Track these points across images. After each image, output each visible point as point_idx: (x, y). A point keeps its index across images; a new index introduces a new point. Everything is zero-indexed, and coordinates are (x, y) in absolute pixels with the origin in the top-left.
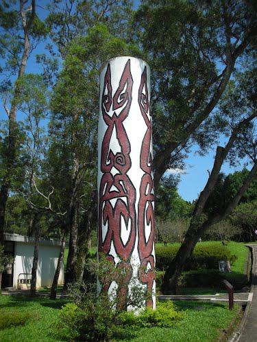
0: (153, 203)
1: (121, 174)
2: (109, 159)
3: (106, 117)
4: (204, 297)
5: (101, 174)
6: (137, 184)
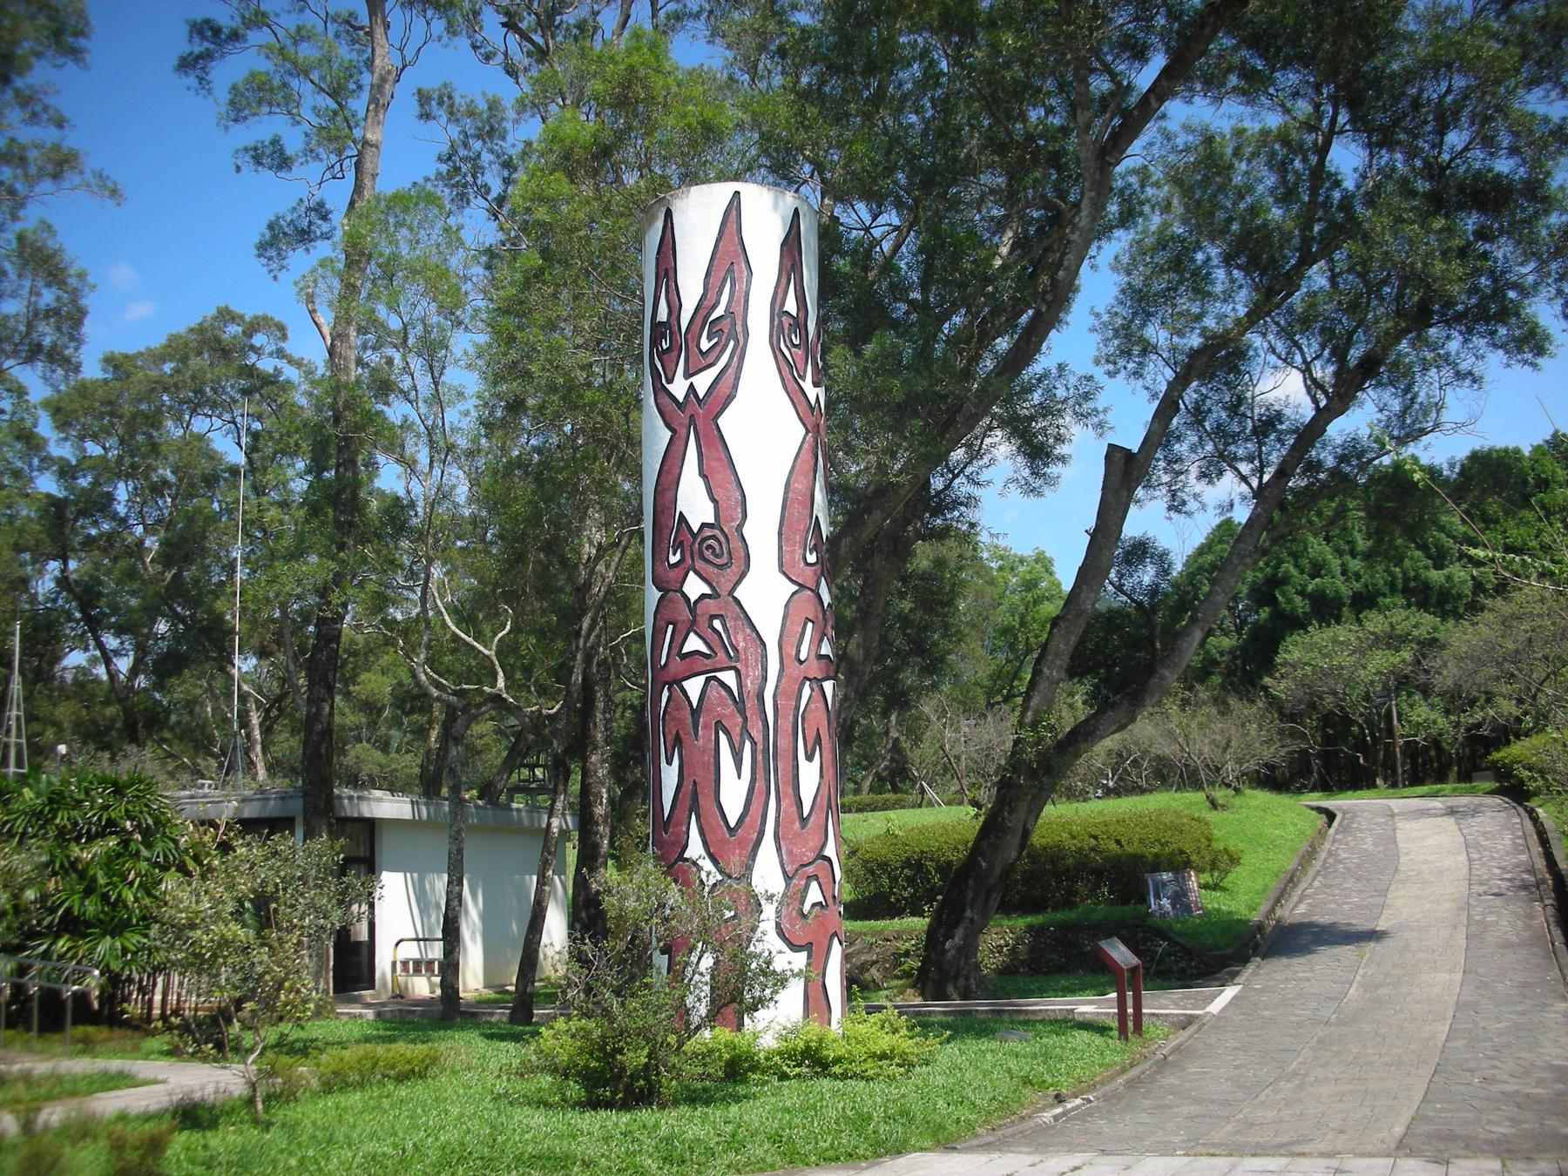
0: (828, 686)
1: (715, 595)
2: (679, 545)
3: (661, 394)
4: (1054, 1005)
5: (653, 595)
6: (770, 630)
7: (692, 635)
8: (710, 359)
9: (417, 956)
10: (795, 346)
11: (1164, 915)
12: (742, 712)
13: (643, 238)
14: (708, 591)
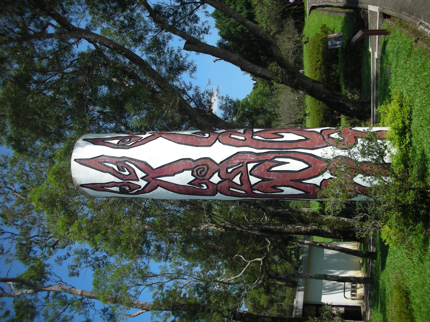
0: (255, 130)
1: (219, 171)
2: (200, 185)
3: (145, 190)
4: (374, 67)
6: (233, 150)
7: (234, 180)
8: (132, 171)
9: (350, 292)
10: (130, 140)
11: (342, 43)
12: (264, 161)
13: (90, 195)
14: (217, 174)
